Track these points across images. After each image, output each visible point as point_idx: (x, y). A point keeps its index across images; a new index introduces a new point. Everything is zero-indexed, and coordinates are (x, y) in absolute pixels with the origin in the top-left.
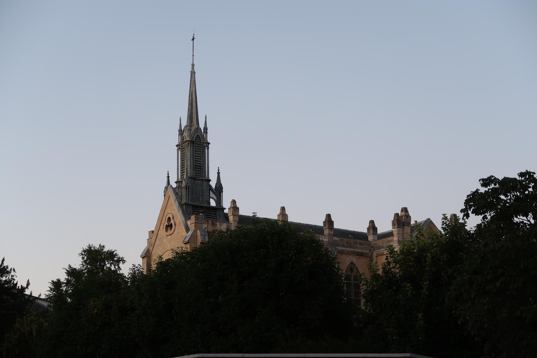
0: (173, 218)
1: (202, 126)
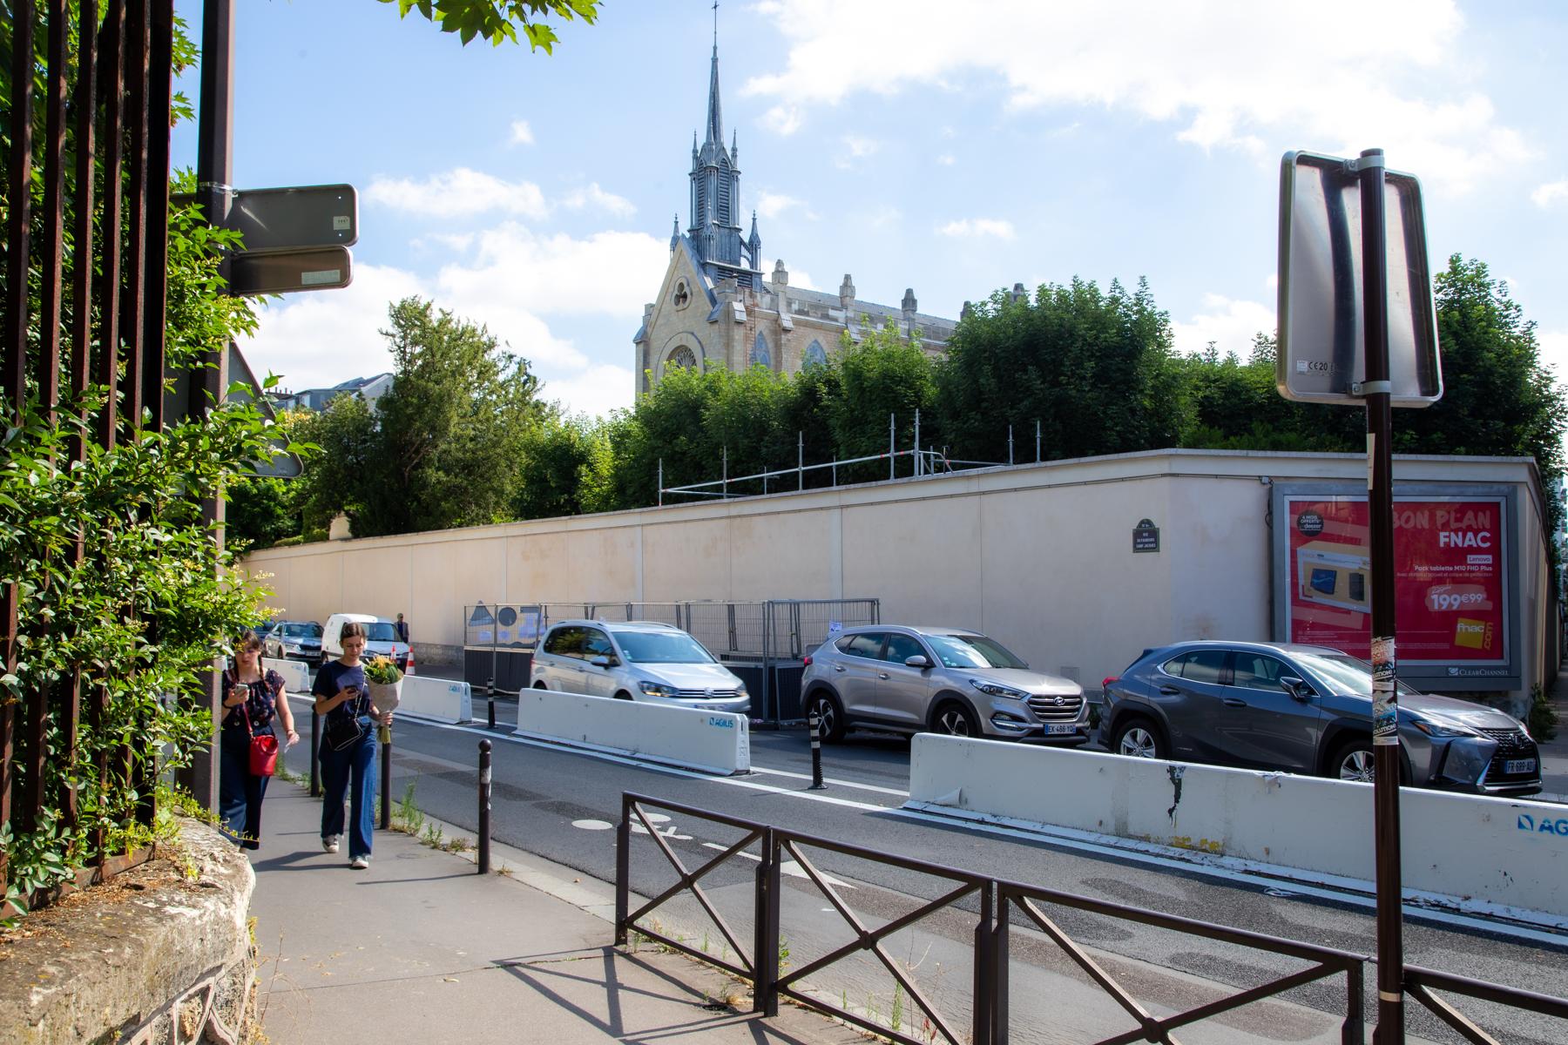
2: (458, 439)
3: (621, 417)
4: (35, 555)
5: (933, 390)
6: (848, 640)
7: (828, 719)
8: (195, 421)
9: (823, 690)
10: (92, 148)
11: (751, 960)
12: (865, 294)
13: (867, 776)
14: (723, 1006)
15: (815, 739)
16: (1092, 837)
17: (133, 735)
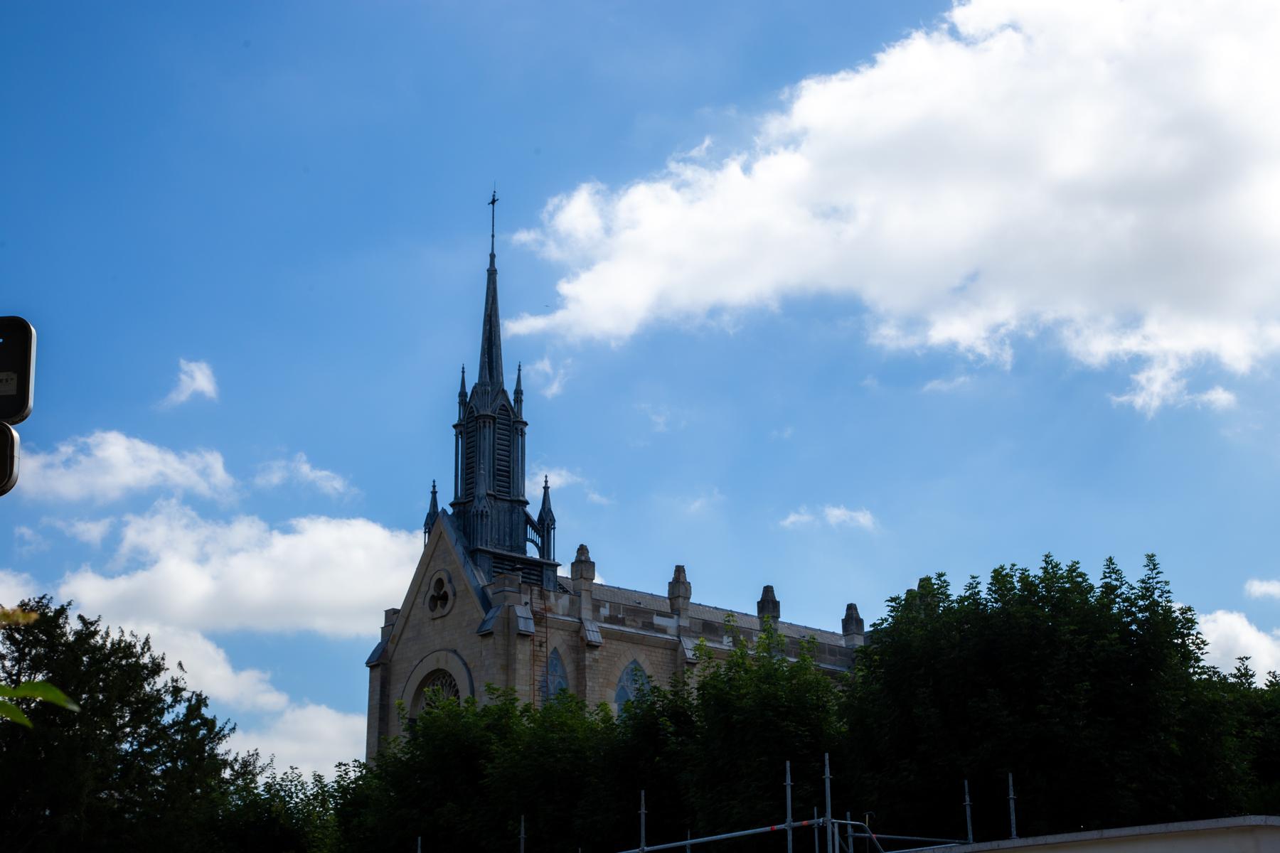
0: (450, 581)
1: (510, 387)
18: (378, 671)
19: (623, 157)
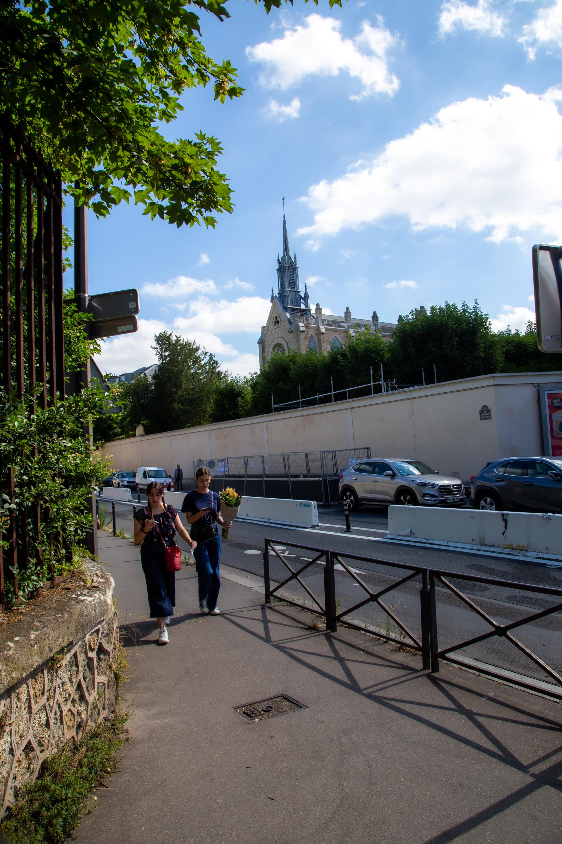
2: (186, 390)
3: (254, 376)
4: (19, 455)
5: (388, 355)
6: (358, 466)
7: (351, 501)
8: (77, 395)
9: (349, 489)
10: (33, 287)
11: (324, 607)
12: (355, 315)
13: (369, 525)
14: (313, 628)
15: (346, 510)
16: (470, 546)
17: (62, 526)
18: (261, 345)
19: (332, 169)
